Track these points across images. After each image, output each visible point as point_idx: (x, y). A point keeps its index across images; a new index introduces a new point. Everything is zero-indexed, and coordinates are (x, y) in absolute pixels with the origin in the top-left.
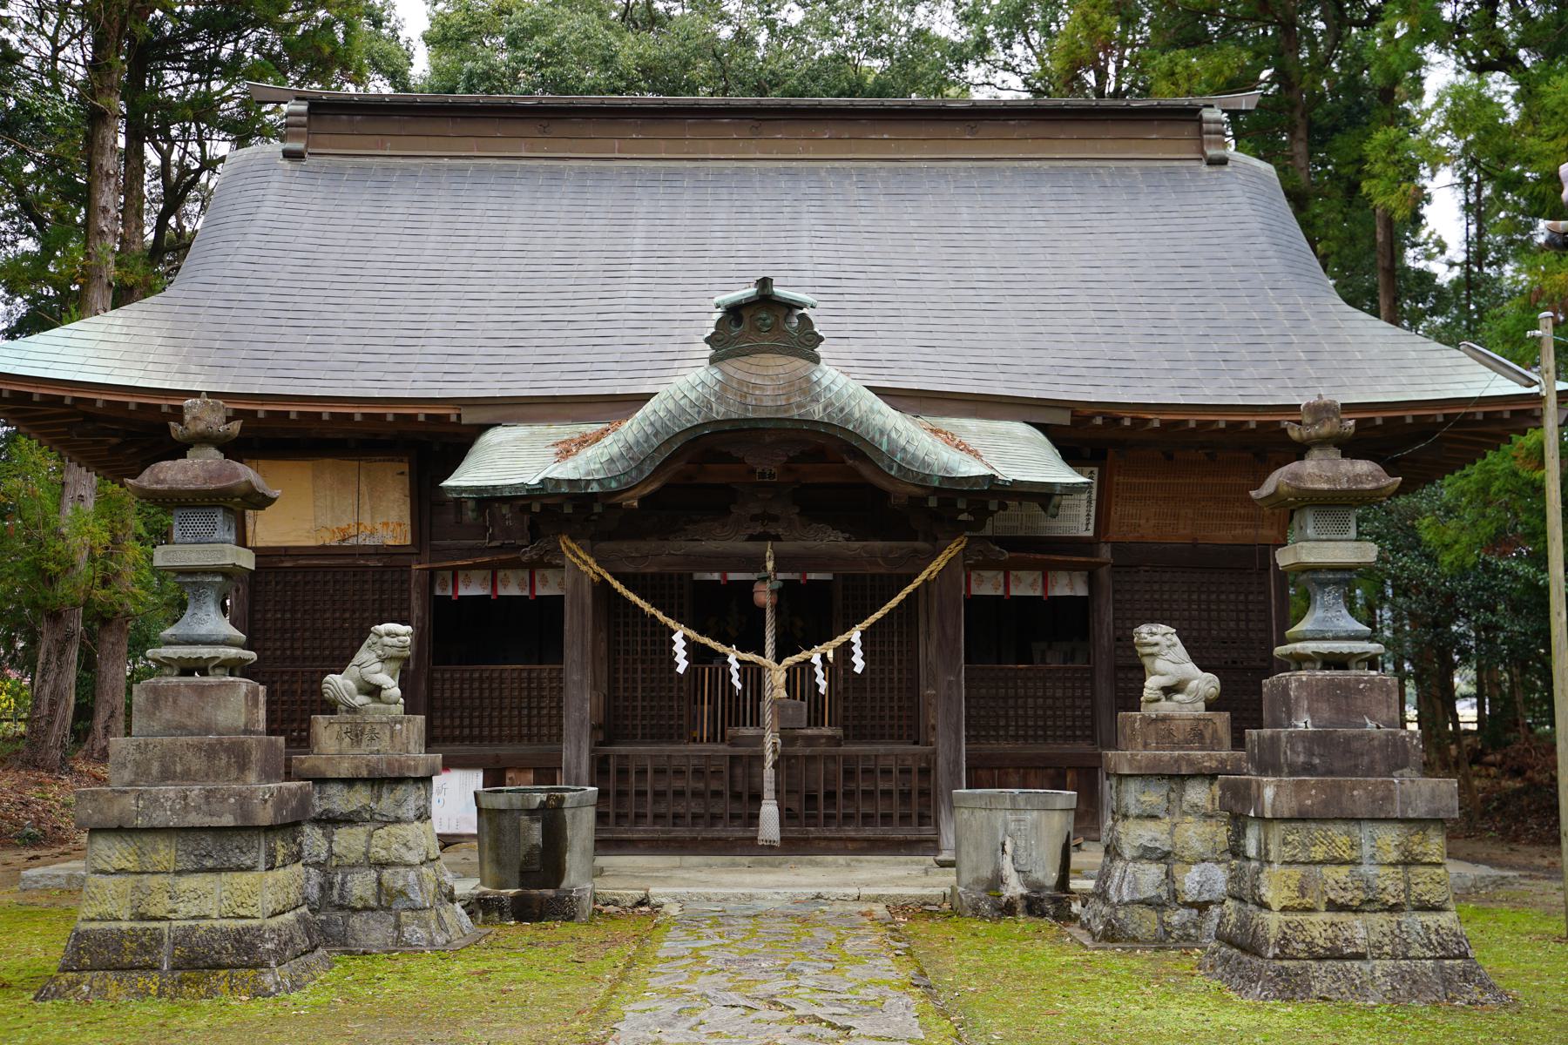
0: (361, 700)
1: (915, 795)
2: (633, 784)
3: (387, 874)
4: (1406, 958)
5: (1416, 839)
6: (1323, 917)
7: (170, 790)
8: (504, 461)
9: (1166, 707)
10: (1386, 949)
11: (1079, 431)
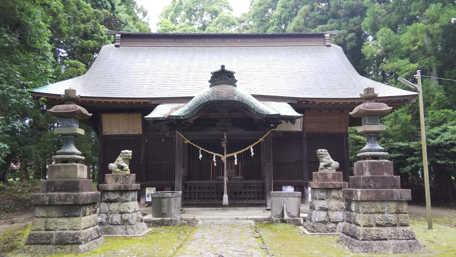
0: (118, 170)
1: (261, 192)
2: (193, 191)
3: (123, 215)
4: (398, 239)
5: (400, 206)
6: (375, 228)
8: (160, 112)
9: (325, 171)
10: (393, 237)
11: (298, 104)
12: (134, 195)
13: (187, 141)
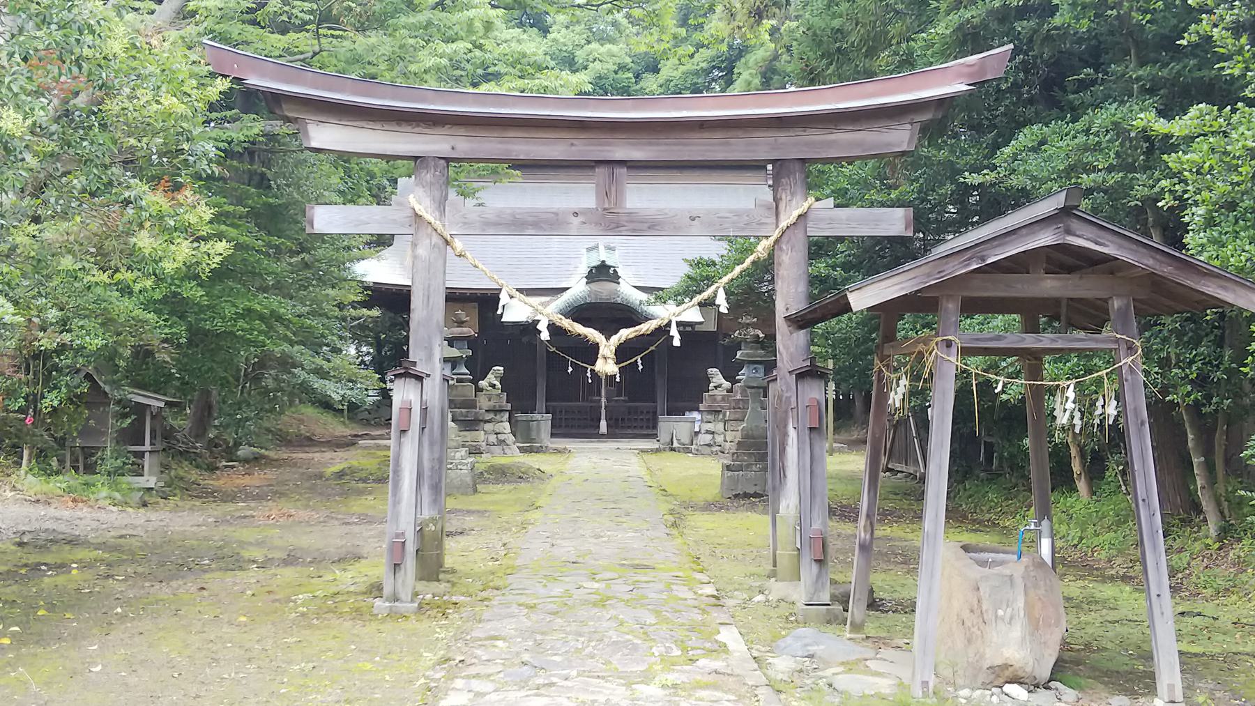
9: (715, 392)
13: (553, 349)
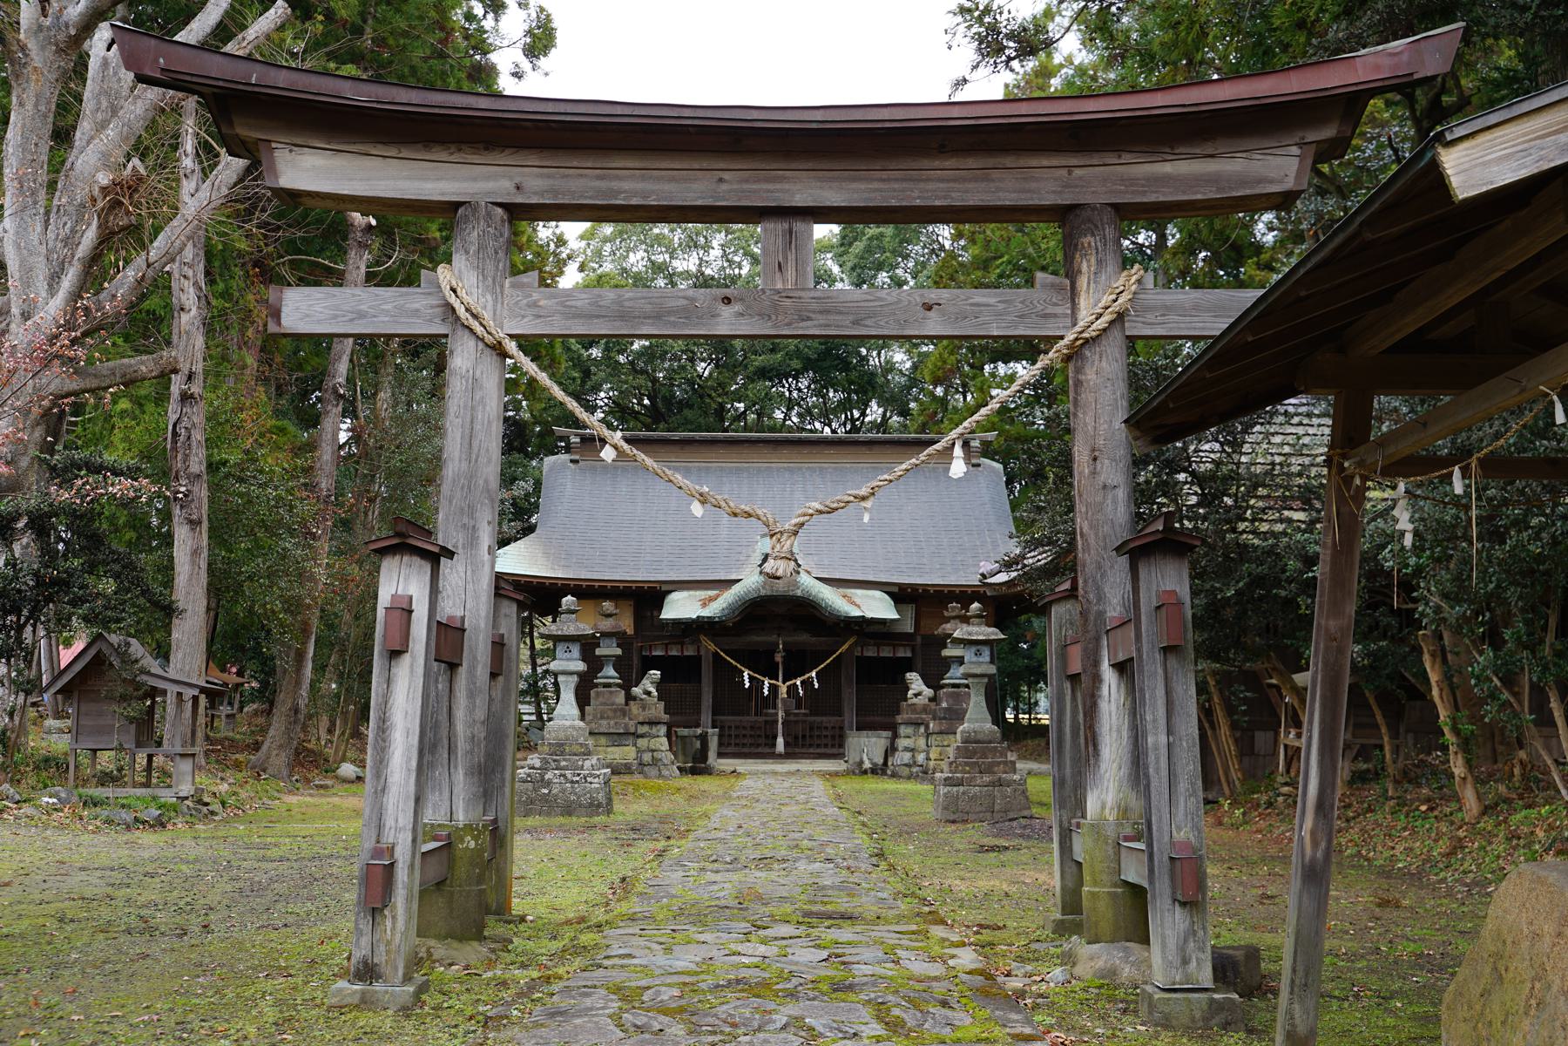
7: (604, 722)
8: (680, 607)
11: (901, 595)
12: (663, 730)
